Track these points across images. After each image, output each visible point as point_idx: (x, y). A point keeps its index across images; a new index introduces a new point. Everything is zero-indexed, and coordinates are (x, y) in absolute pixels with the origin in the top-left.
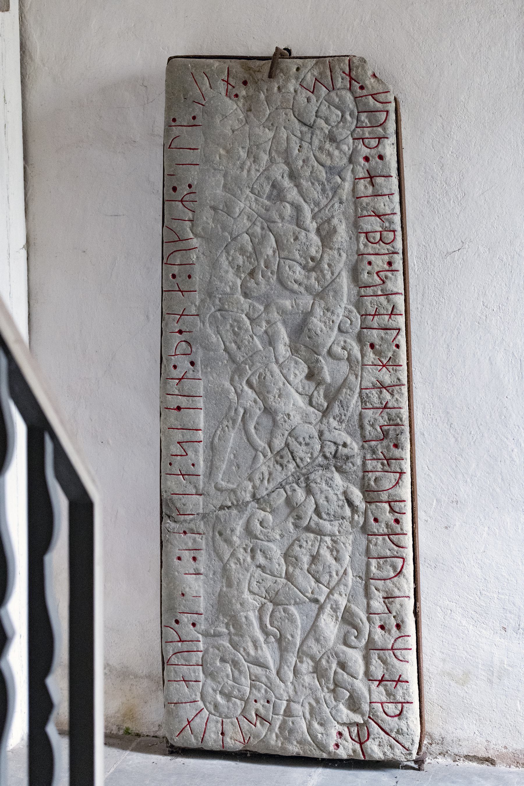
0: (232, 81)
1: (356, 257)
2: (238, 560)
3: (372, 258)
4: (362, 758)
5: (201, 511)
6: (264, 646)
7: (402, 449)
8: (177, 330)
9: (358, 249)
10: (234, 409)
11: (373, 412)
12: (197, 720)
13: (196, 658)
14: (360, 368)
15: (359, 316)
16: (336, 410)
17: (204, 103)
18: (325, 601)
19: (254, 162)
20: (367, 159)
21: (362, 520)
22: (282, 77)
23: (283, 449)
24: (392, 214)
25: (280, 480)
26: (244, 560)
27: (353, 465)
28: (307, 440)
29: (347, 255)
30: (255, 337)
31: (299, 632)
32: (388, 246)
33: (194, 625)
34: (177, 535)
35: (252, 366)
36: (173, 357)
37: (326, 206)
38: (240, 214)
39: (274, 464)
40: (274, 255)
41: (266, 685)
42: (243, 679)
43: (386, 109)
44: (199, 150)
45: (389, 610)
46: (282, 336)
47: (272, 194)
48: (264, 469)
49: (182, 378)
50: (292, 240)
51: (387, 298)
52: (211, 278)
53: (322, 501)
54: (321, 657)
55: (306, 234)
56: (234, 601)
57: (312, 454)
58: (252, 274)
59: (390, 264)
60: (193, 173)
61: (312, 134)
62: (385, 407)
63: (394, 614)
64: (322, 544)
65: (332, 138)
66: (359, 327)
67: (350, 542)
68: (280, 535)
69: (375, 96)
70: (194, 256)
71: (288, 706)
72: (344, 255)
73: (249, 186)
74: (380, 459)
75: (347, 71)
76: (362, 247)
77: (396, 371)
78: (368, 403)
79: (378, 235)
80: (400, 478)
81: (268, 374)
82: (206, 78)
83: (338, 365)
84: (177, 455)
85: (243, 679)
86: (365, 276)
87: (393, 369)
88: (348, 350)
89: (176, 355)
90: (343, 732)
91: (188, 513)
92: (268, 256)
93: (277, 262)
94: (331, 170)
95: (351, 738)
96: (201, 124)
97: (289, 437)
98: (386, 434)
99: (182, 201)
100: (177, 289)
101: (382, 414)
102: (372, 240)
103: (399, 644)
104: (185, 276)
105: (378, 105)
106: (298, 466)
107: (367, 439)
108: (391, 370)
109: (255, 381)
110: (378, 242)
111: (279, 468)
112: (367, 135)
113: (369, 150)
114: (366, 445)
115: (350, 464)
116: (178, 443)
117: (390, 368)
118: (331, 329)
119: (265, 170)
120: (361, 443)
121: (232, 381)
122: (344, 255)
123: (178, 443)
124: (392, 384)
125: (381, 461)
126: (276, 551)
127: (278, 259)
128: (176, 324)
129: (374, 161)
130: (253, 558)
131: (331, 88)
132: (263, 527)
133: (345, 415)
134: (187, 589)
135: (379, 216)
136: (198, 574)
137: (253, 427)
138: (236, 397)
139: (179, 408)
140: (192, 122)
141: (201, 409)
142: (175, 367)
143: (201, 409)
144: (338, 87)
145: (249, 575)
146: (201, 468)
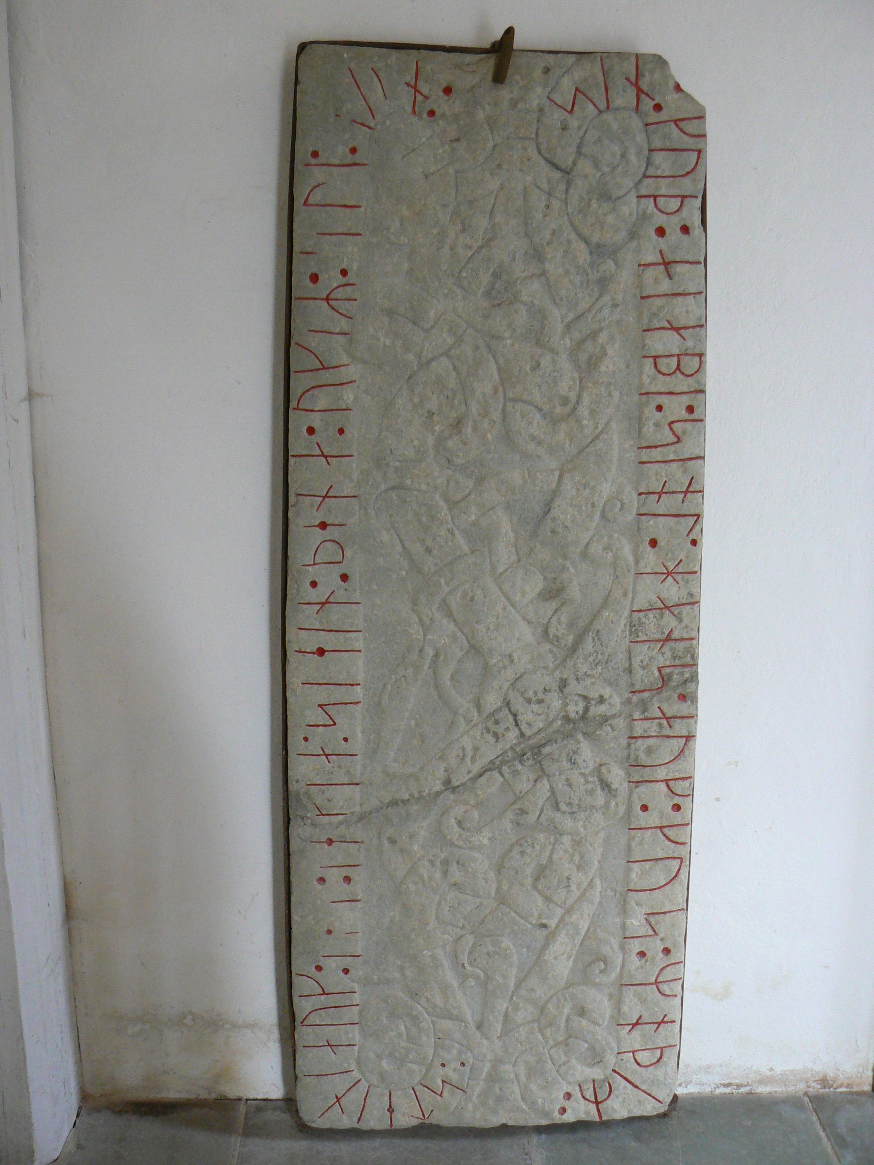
0: (424, 88)
1: (636, 398)
2: (421, 877)
3: (663, 400)
4: (598, 1120)
5: (357, 809)
6: (459, 995)
7: (692, 702)
8: (317, 523)
9: (641, 385)
10: (417, 650)
11: (649, 648)
12: (353, 1095)
13: (353, 1014)
14: (631, 579)
15: (635, 496)
16: (589, 646)
17: (372, 125)
18: (557, 927)
19: (463, 230)
20: (661, 232)
21: (622, 810)
22: (517, 83)
23: (500, 709)
24: (697, 326)
25: (492, 757)
26: (430, 878)
27: (613, 730)
28: (540, 695)
29: (621, 394)
30: (456, 532)
31: (514, 971)
32: (690, 380)
33: (346, 971)
34: (318, 845)
35: (452, 579)
36: (310, 568)
37: (589, 310)
38: (436, 323)
39: (482, 734)
40: (496, 393)
41: (459, 1043)
42: (424, 1038)
43: (700, 146)
44: (362, 209)
45: (654, 931)
46: (504, 530)
47: (493, 288)
48: (467, 742)
49: (327, 602)
50: (528, 368)
51: (682, 466)
52: (380, 434)
53: (560, 785)
54: (548, 1001)
55: (553, 360)
56: (413, 936)
57: (548, 716)
58: (457, 425)
59: (690, 409)
60: (349, 249)
61: (569, 184)
62: (668, 639)
63: (662, 935)
64: (556, 847)
65: (605, 196)
66: (634, 512)
67: (601, 841)
68: (490, 839)
69: (681, 124)
70: (348, 396)
71: (494, 1068)
72: (616, 394)
73: (453, 275)
74: (657, 718)
75: (633, 79)
76: (646, 380)
77: (687, 582)
78: (640, 634)
79: (674, 362)
80: (685, 744)
81: (479, 592)
82: (376, 79)
83: (595, 575)
84: (318, 726)
85: (424, 1038)
86: (649, 429)
87: (683, 579)
88: (614, 550)
89: (315, 564)
90: (573, 1093)
91: (335, 812)
92: (484, 395)
93: (501, 406)
94: (598, 251)
95: (584, 1097)
96: (366, 162)
97: (511, 692)
98: (665, 680)
99: (327, 299)
100: (319, 452)
101: (663, 650)
102: (664, 370)
103: (668, 974)
104: (333, 430)
105: (686, 139)
106: (522, 734)
107: (637, 688)
108: (680, 581)
109: (455, 603)
110: (674, 372)
111: (490, 738)
112: (663, 192)
113: (665, 217)
114: (635, 698)
115: (609, 728)
116: (320, 706)
117: (679, 578)
118: (590, 516)
119: (480, 248)
120: (626, 695)
121: (415, 602)
122: (616, 394)
123: (320, 706)
124: (679, 603)
125: (657, 721)
126: (481, 864)
127: (502, 400)
128: (315, 513)
129: (674, 235)
130: (445, 873)
131: (603, 106)
132: (463, 829)
133: (602, 654)
134: (337, 924)
135: (677, 330)
136: (353, 901)
137: (448, 676)
138: (421, 630)
139: (321, 652)
140: (350, 159)
141: (360, 651)
142: (314, 584)
143: (360, 651)
144: (616, 106)
145: (438, 897)
146: (358, 744)
